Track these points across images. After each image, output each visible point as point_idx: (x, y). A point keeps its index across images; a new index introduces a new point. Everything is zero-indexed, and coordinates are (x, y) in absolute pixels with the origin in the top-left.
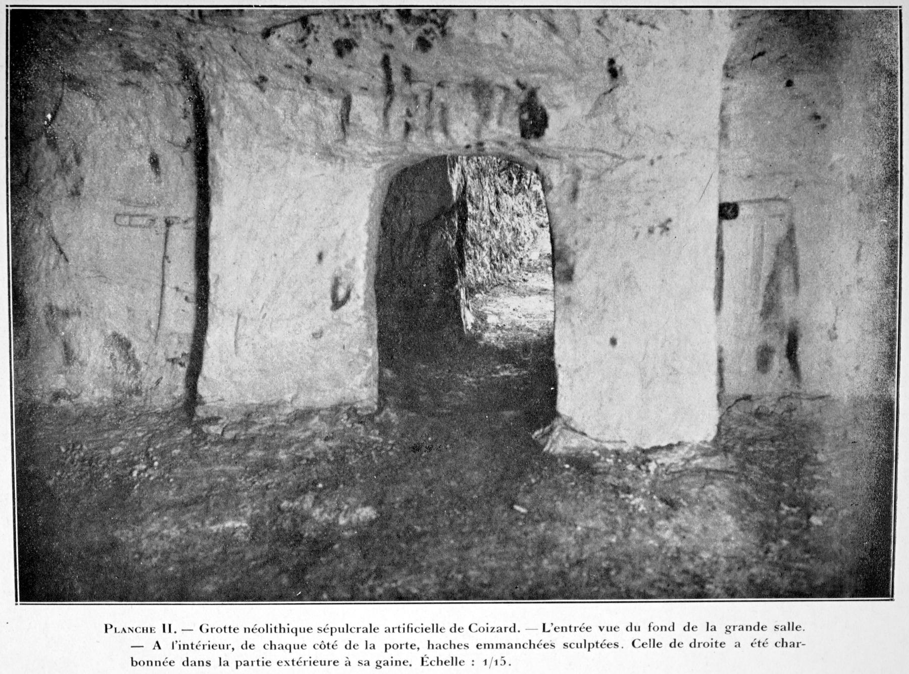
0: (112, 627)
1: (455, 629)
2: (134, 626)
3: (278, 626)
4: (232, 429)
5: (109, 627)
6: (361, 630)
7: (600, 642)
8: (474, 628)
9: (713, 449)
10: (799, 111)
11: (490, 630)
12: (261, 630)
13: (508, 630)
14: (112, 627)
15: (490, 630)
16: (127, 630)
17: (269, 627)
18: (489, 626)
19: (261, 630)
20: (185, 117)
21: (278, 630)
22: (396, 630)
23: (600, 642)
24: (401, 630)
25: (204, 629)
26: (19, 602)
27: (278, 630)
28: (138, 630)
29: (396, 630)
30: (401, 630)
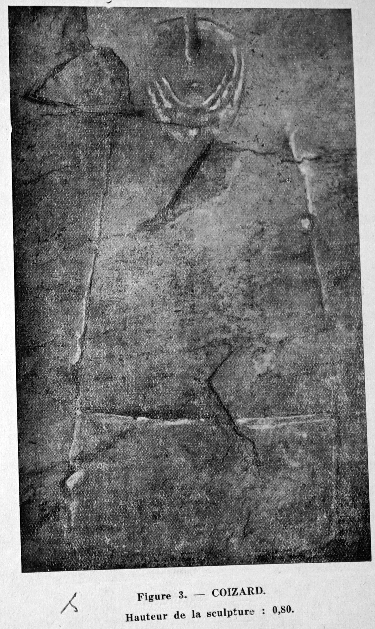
11: (232, 592)
15: (232, 592)
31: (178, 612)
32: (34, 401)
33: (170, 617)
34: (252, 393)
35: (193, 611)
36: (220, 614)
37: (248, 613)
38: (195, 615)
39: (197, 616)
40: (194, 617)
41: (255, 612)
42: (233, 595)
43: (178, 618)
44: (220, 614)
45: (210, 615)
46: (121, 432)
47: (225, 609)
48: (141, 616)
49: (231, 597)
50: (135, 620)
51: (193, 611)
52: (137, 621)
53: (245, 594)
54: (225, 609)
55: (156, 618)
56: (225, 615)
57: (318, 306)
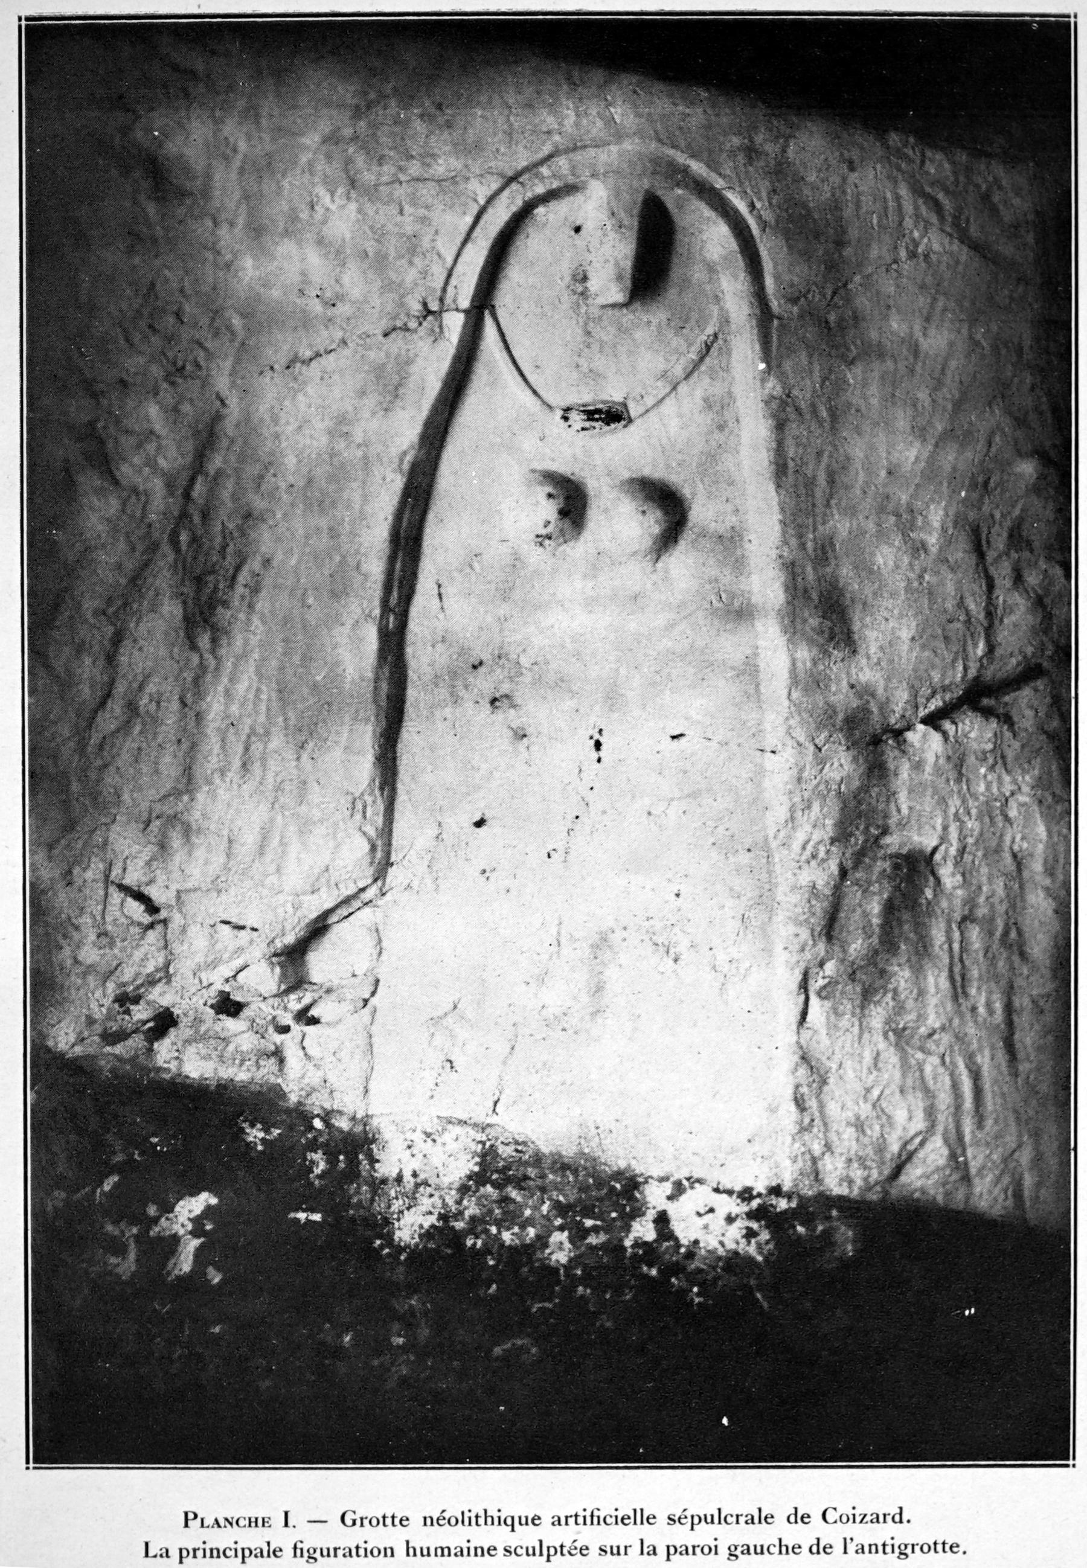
0: (196, 1516)
1: (800, 1518)
2: (233, 1514)
3: (482, 1514)
4: (1051, 846)
5: (191, 1516)
6: (742, 1520)
7: (568, 1544)
8: (831, 1516)
9: (539, 1255)
10: (904, 654)
11: (858, 1519)
12: (453, 1521)
13: (889, 1518)
14: (196, 1516)
15: (858, 1519)
16: (222, 1522)
17: (467, 1514)
18: (857, 1512)
19: (453, 1521)
20: (378, 455)
21: (481, 1521)
22: (571, 1521)
23: (568, 1544)
24: (580, 1520)
25: (348, 1520)
26: (31, 1465)
27: (481, 1521)
28: (242, 1522)
29: (571, 1521)
30: (580, 1520)
31: (818, 1539)
32: (410, 55)
33: (594, 1551)
34: (175, 364)
35: (642, 1541)
36: (873, 1548)
37: (698, 1550)
38: (646, 1550)
39: (648, 1554)
40: (642, 1553)
41: (284, 1552)
42: (861, 1522)
43: (818, 1553)
44: (873, 1548)
45: (510, 1552)
46: (94, 380)
47: (541, 1542)
48: (877, 1552)
49: (857, 1525)
50: (456, 1555)
51: (642, 1541)
52: (861, 1555)
53: (219, 1526)
54: (541, 1542)
55: (453, 1552)
56: (541, 1554)
57: (901, 616)
